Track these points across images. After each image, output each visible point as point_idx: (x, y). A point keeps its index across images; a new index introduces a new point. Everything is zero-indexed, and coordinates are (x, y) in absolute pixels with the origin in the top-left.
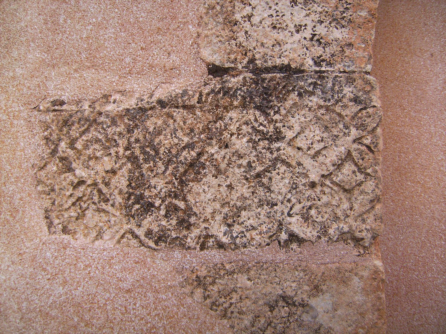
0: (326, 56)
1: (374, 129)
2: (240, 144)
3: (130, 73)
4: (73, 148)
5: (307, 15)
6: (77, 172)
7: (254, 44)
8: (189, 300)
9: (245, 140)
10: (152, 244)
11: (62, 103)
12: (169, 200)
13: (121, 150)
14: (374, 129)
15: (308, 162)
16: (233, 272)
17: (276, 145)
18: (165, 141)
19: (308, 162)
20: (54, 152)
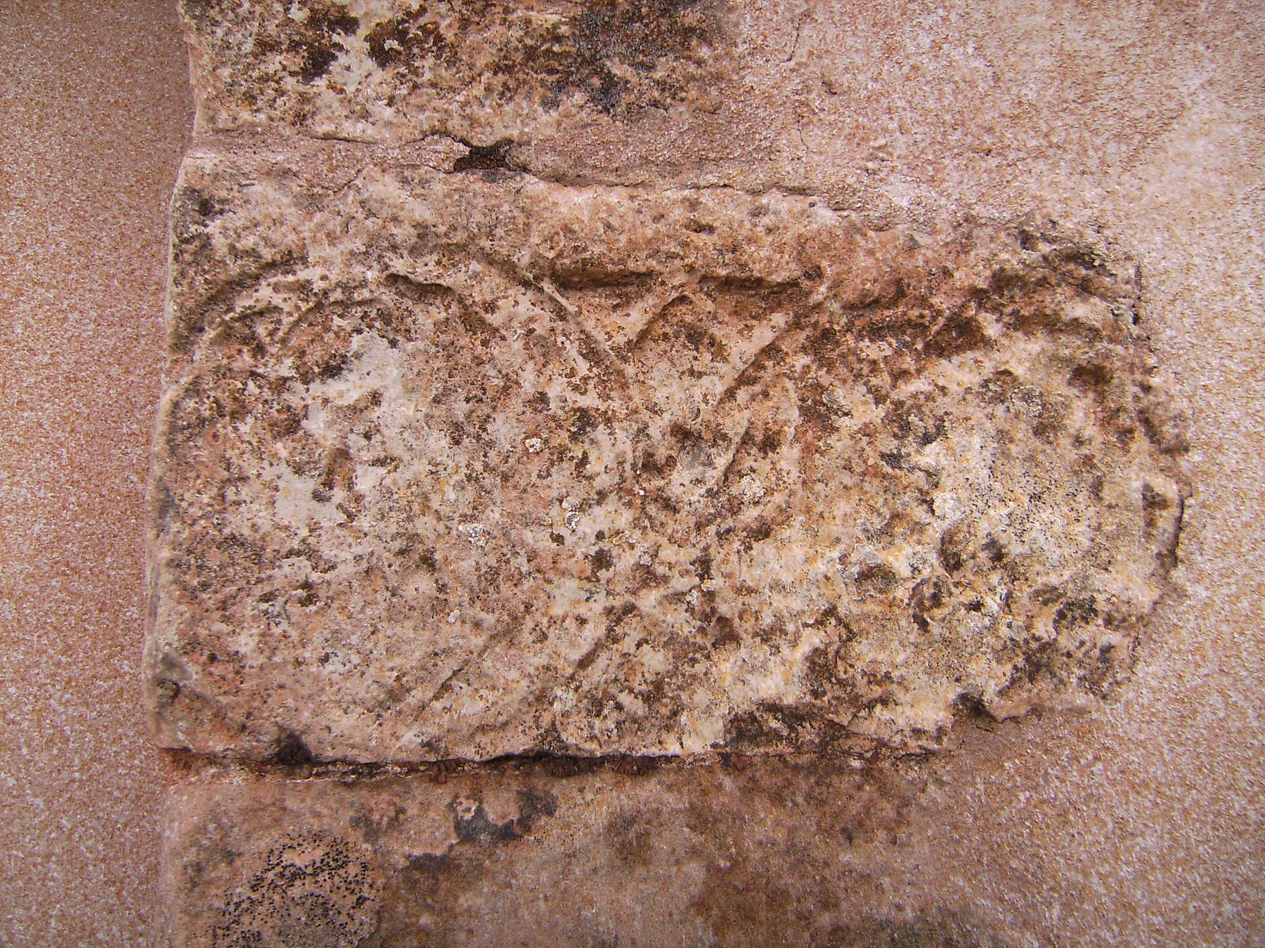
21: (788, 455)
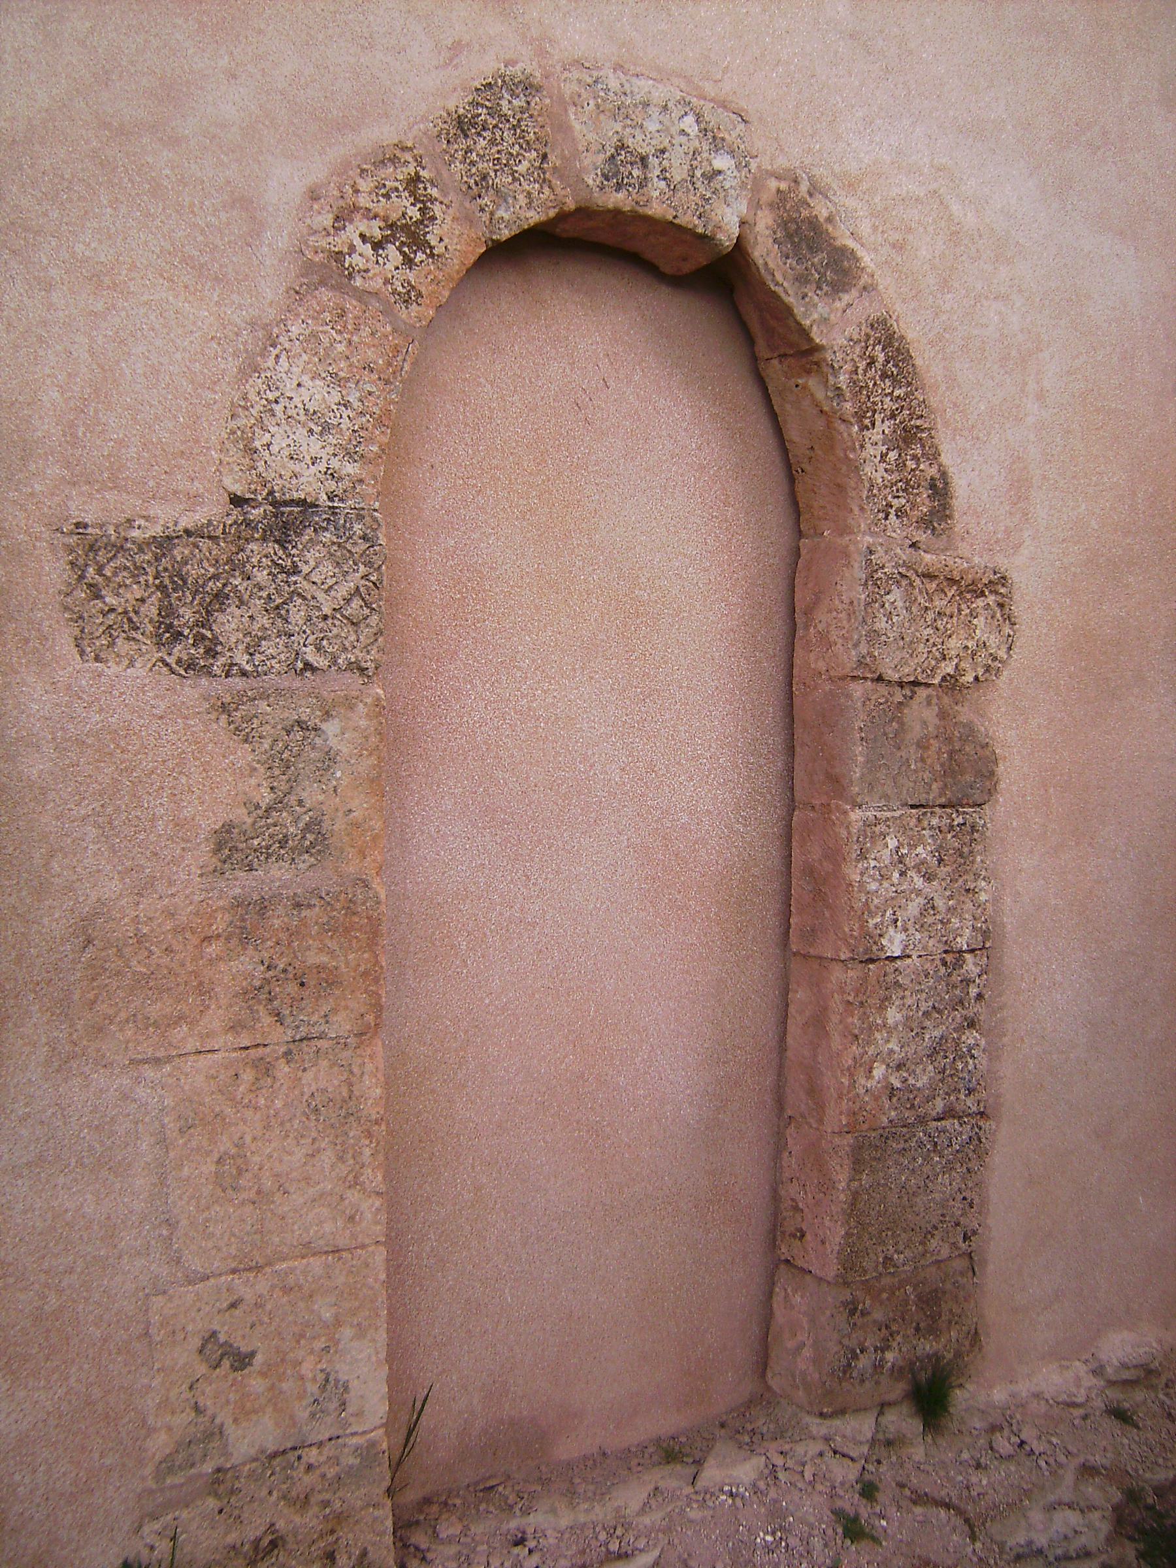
0: (339, 492)
1: (380, 566)
2: (261, 576)
3: (154, 497)
4: (101, 575)
5: (323, 447)
6: (107, 600)
7: (273, 475)
8: (215, 726)
9: (265, 572)
10: (183, 673)
11: (86, 526)
12: (196, 629)
13: (151, 579)
14: (380, 566)
15: (321, 596)
16: (255, 699)
17: (293, 579)
18: (193, 571)
19: (321, 596)
20: (82, 577)
21: (955, 619)
